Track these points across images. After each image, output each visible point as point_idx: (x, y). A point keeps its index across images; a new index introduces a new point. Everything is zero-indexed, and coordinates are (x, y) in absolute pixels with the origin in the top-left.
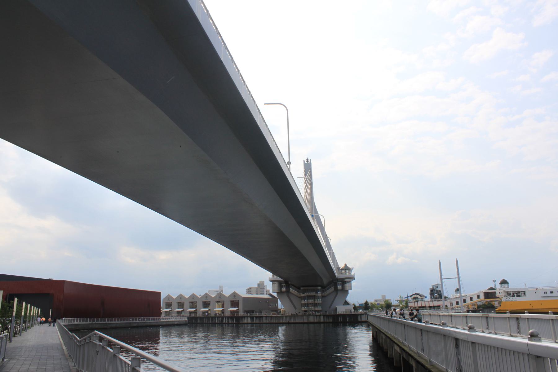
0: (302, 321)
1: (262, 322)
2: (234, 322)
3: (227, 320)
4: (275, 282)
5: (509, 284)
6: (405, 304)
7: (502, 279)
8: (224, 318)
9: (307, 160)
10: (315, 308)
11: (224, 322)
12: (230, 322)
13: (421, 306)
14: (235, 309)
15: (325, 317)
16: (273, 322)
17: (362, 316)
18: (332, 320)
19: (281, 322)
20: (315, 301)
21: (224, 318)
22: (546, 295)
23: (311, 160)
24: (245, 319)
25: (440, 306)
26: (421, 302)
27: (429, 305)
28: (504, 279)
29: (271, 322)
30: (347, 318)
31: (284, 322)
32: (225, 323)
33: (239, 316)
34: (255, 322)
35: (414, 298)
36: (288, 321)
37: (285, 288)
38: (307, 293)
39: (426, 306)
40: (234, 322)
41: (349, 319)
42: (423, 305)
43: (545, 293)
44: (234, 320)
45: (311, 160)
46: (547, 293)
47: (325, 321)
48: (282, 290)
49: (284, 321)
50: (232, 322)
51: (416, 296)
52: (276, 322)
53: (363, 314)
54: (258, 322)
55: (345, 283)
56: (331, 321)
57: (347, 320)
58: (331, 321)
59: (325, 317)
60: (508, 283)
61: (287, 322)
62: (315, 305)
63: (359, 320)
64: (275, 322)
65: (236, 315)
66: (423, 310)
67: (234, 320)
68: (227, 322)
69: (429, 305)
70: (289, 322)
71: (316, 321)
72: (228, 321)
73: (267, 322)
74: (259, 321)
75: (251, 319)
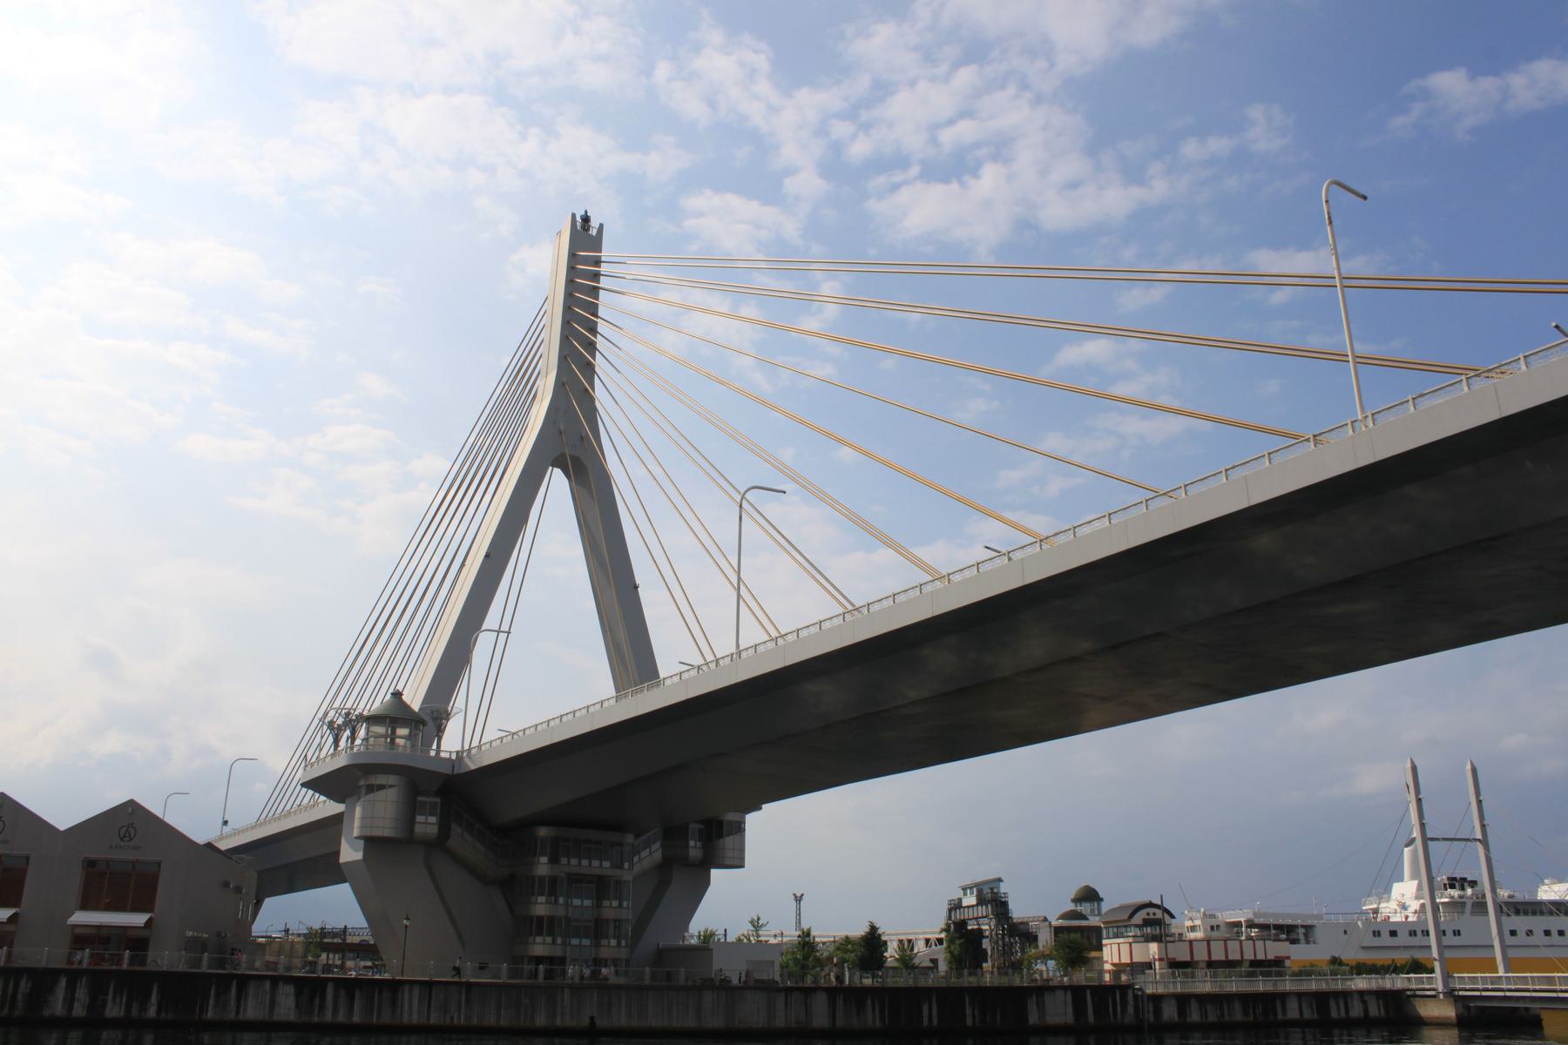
0: (690, 1022)
1: (386, 1019)
2: (152, 1012)
3: (81, 994)
4: (381, 779)
5: (1103, 903)
6: (577, 967)
7: (1083, 885)
8: (63, 982)
9: (586, 219)
10: (597, 945)
11: (57, 1006)
12: (114, 1010)
13: (1223, 958)
14: (138, 919)
15: (840, 1002)
16: (475, 1022)
17: (1048, 999)
18: (882, 1018)
19: (541, 1021)
20: (599, 906)
21: (63, 982)
22: (1377, 942)
23: (601, 226)
24: (251, 990)
25: (1283, 961)
26: (1130, 944)
27: (1255, 956)
28: (1087, 886)
29: (460, 1019)
30: (968, 1011)
31: (558, 1022)
32: (66, 1023)
33: (150, 967)
34: (328, 1017)
35: (1147, 922)
36: (592, 1018)
37: (433, 819)
38: (574, 861)
39: (1196, 959)
40: (152, 1012)
41: (976, 1012)
42: (1234, 955)
43: (1377, 934)
44: (154, 999)
45: (601, 226)
46: (1382, 933)
47: (840, 1023)
48: (419, 829)
49: (565, 1020)
50: (135, 1013)
51: (1152, 916)
52: (503, 1022)
53: (1053, 989)
54: (356, 1019)
55: (720, 836)
56: (878, 1024)
57: (969, 1022)
58: (878, 1024)
59: (840, 1002)
60: (1102, 900)
61: (586, 1022)
62: (598, 929)
63: (1033, 1019)
64: (491, 1020)
65: (132, 960)
66: (1269, 974)
67: (154, 999)
68: (79, 1011)
69: (1255, 956)
70: (601, 1023)
71: (780, 1022)
72: (96, 1004)
73: (434, 1019)
74: (1245, 1013)
75: (298, 995)
